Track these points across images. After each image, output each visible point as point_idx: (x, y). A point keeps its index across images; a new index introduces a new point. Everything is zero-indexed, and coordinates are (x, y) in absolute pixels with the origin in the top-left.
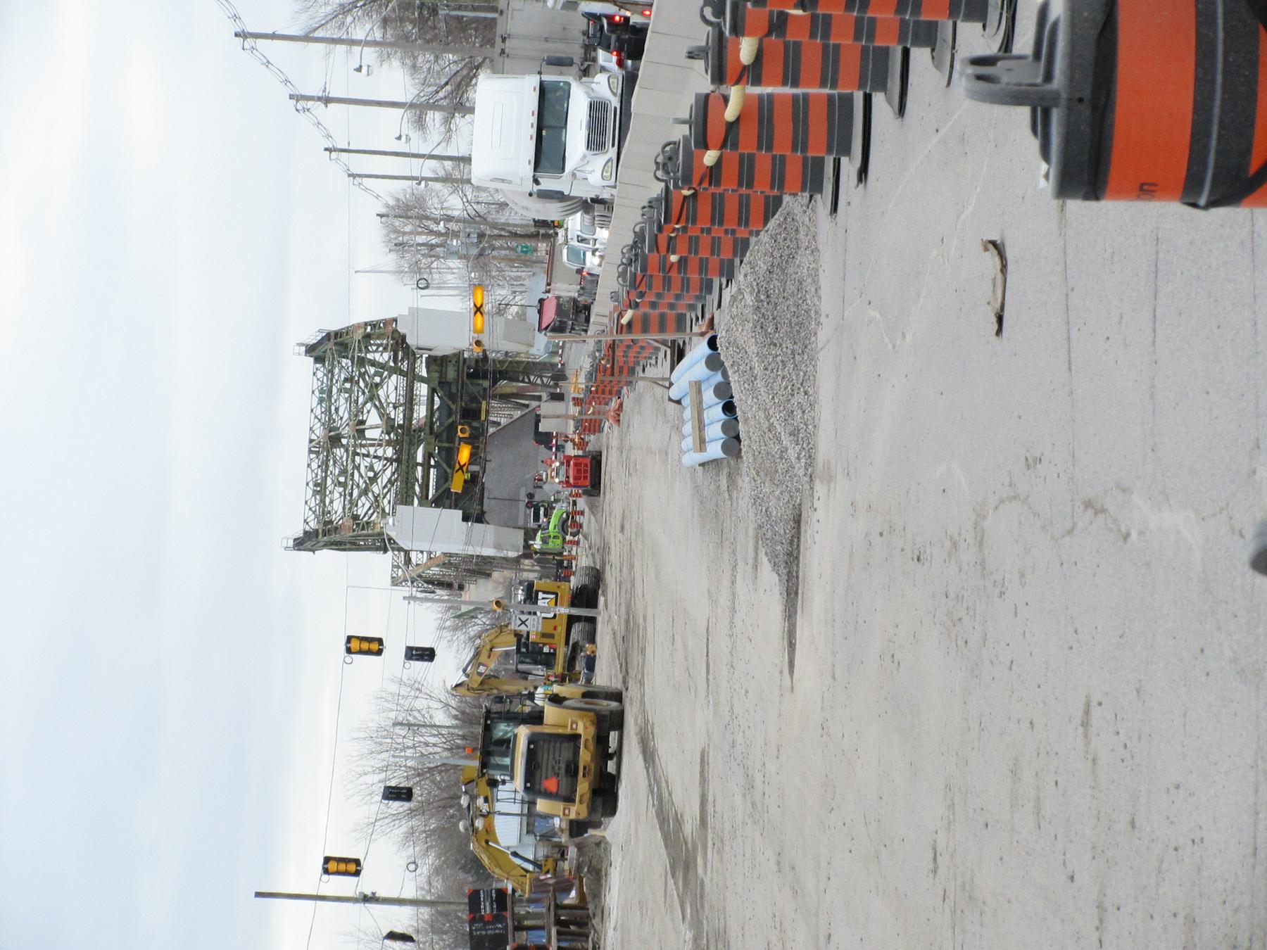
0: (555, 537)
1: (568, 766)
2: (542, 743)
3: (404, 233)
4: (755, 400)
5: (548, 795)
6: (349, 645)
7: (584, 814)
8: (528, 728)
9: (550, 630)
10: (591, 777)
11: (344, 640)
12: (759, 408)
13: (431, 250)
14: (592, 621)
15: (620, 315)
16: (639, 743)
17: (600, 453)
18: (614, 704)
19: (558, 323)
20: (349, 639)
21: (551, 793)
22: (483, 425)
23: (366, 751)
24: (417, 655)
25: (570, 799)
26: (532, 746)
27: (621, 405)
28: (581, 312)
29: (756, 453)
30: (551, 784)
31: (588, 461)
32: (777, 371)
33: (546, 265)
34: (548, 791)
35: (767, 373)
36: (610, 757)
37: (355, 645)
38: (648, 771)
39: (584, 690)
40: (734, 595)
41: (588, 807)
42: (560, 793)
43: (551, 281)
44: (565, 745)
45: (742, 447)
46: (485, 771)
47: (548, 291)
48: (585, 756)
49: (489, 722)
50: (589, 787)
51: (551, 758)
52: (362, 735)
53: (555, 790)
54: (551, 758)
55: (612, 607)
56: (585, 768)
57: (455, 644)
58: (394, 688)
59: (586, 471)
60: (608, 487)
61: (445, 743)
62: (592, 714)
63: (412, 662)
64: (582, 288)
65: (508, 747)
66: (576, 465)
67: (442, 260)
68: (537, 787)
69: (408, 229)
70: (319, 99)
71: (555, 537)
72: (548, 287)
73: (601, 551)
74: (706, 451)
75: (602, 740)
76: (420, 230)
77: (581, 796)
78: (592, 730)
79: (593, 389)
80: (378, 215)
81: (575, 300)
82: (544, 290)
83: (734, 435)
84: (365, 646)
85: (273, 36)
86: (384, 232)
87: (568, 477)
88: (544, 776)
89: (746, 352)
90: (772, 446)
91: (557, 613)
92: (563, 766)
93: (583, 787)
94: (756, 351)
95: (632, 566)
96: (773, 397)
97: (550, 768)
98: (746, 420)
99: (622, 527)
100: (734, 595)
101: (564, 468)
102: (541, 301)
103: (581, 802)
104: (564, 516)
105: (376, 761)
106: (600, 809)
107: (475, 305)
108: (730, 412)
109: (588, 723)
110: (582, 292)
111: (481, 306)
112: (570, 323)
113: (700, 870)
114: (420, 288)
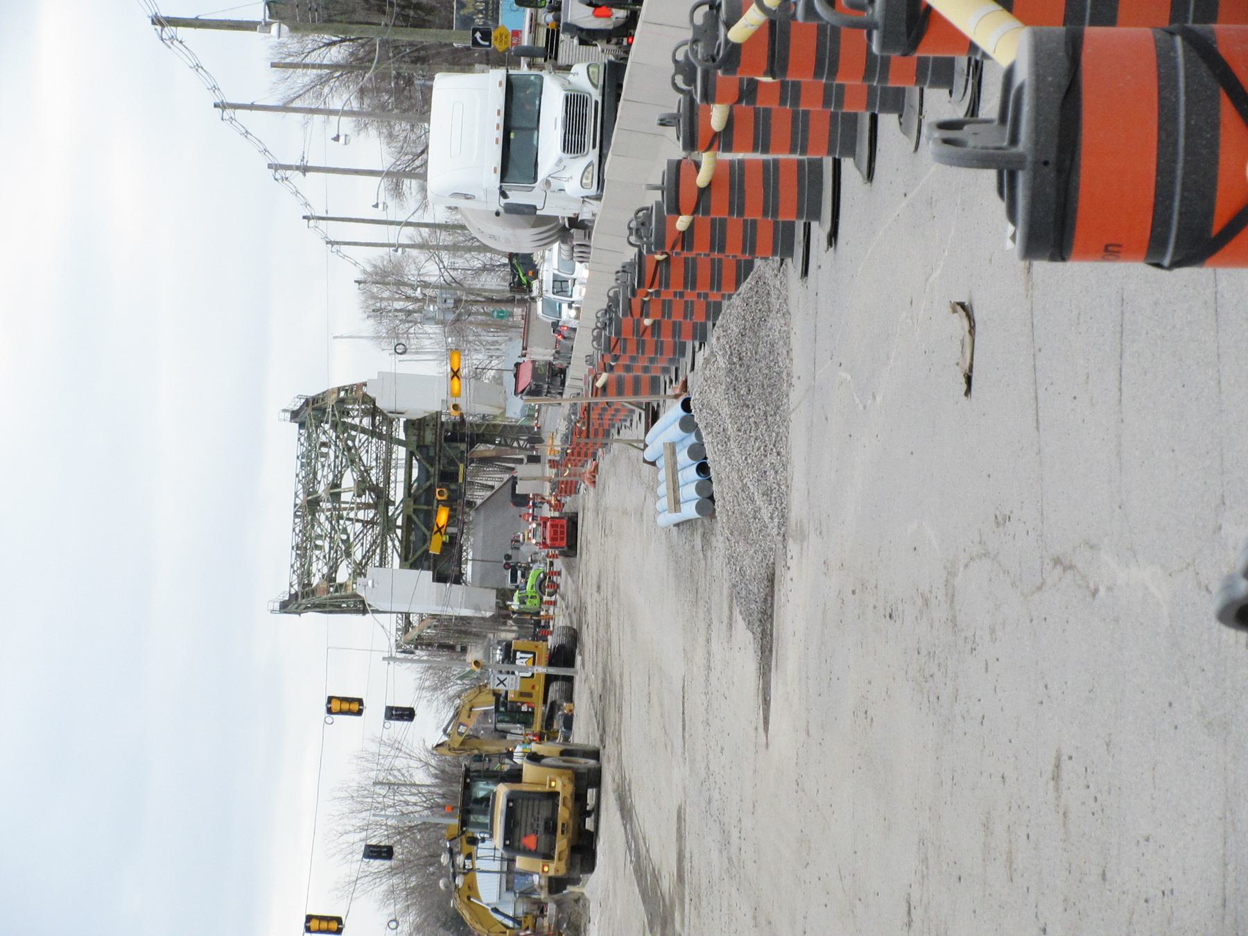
0: (532, 597)
1: (546, 823)
2: (520, 801)
3: (382, 299)
4: (728, 461)
5: (527, 852)
6: (308, 925)
8: (507, 786)
9: (529, 690)
10: (570, 835)
11: (325, 701)
12: (733, 469)
14: (569, 680)
15: (595, 379)
18: (592, 762)
19: (533, 387)
20: (330, 699)
21: (530, 851)
22: (461, 488)
23: (347, 811)
24: (396, 715)
25: (548, 856)
26: (511, 804)
27: (597, 467)
28: (556, 375)
29: (730, 513)
30: (530, 842)
31: (564, 522)
34: (527, 849)
36: (589, 814)
37: (336, 706)
38: (625, 828)
39: (562, 748)
43: (527, 345)
44: (544, 803)
45: (716, 507)
46: (464, 829)
48: (564, 814)
49: (468, 780)
51: (530, 813)
52: (344, 794)
53: (533, 848)
54: (530, 813)
55: (589, 666)
56: (563, 825)
57: (435, 703)
58: (374, 748)
61: (425, 802)
63: (392, 722)
65: (487, 805)
66: (552, 526)
67: (419, 325)
69: (386, 294)
70: (298, 168)
71: (532, 597)
72: (524, 352)
73: (578, 611)
75: (579, 797)
76: (397, 296)
77: (560, 854)
79: (569, 451)
80: (356, 282)
81: (550, 364)
82: (520, 355)
83: (708, 495)
84: (345, 706)
85: (252, 107)
86: (362, 298)
87: (545, 538)
91: (535, 672)
92: (542, 823)
93: (562, 844)
94: (728, 413)
95: (608, 626)
98: (720, 481)
99: (599, 587)
101: (540, 529)
102: (517, 365)
103: (560, 859)
104: (542, 575)
105: (357, 820)
106: (578, 867)
107: (452, 370)
108: (703, 473)
109: (566, 781)
110: (557, 356)
111: (458, 370)
112: (546, 386)
114: (398, 353)
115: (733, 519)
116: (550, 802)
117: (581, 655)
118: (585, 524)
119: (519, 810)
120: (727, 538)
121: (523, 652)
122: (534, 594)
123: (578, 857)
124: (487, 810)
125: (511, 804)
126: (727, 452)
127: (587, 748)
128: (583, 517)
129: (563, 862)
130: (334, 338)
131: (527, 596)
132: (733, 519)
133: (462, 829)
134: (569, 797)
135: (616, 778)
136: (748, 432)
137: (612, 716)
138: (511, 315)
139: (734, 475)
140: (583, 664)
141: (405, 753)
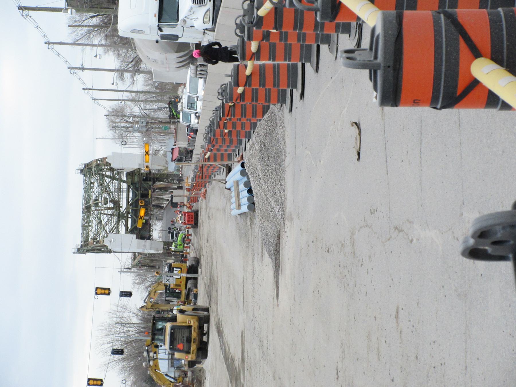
0: (180, 245)
3: (116, 122)
5: (179, 351)
6: (96, 291)
7: (194, 358)
8: (170, 323)
9: (179, 284)
11: (94, 289)
13: (127, 129)
14: (196, 279)
15: (205, 154)
16: (216, 329)
17: (198, 210)
18: (206, 313)
20: (97, 289)
24: (124, 295)
25: (188, 352)
27: (206, 191)
28: (189, 153)
29: (261, 210)
30: (180, 346)
31: (193, 214)
32: (269, 176)
33: (174, 134)
35: (265, 177)
36: (204, 334)
37: (99, 291)
38: (220, 340)
40: (253, 267)
41: (196, 355)
42: (184, 350)
44: (186, 330)
46: (153, 341)
47: (175, 145)
48: (194, 335)
49: (154, 321)
50: (196, 348)
51: (180, 334)
52: (102, 328)
54: (180, 334)
55: (204, 273)
58: (115, 308)
59: (192, 218)
60: (201, 224)
61: (136, 330)
62: (197, 317)
63: (122, 298)
64: (189, 144)
65: (162, 332)
66: (188, 215)
68: (175, 347)
69: (117, 120)
70: (80, 69)
71: (180, 245)
72: (175, 143)
73: (199, 250)
74: (241, 209)
75: (201, 328)
77: (193, 351)
78: (197, 324)
79: (194, 184)
80: (105, 115)
84: (103, 291)
85: (60, 43)
86: (108, 122)
88: (177, 343)
89: (256, 169)
90: (268, 206)
92: (185, 339)
93: (194, 347)
95: (212, 256)
96: (268, 187)
97: (180, 340)
99: (208, 241)
100: (253, 267)
101: (183, 217)
102: (173, 149)
103: (193, 353)
104: (184, 236)
106: (201, 356)
107: (145, 151)
111: (148, 151)
112: (184, 158)
113: (242, 380)
114: (123, 145)
115: (263, 212)
116: (189, 330)
117: (201, 269)
118: (201, 215)
119: (175, 334)
120: (261, 220)
121: (176, 268)
122: (181, 244)
123: (200, 353)
124: (162, 334)
125: (172, 331)
126: (260, 184)
127: (204, 307)
128: (201, 212)
129: (194, 354)
130: (96, 139)
131: (178, 245)
132: (263, 212)
133: (152, 342)
134: (196, 328)
135: (216, 319)
136: (268, 176)
137: (214, 294)
138: (170, 128)
139: (263, 194)
140: (201, 273)
141: (128, 310)
